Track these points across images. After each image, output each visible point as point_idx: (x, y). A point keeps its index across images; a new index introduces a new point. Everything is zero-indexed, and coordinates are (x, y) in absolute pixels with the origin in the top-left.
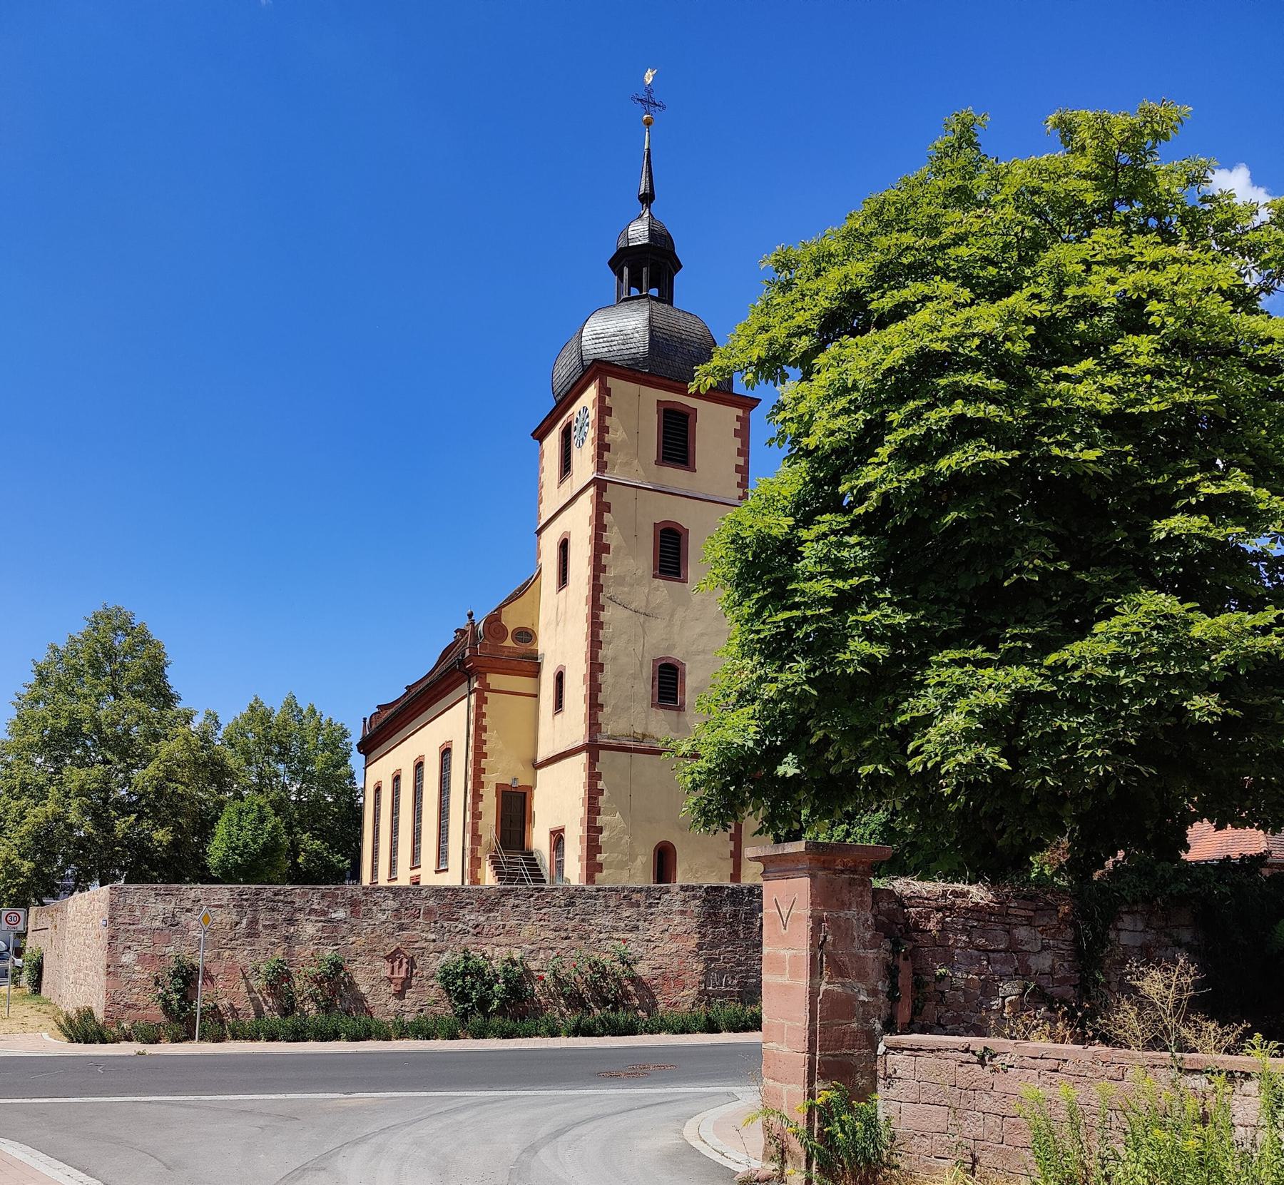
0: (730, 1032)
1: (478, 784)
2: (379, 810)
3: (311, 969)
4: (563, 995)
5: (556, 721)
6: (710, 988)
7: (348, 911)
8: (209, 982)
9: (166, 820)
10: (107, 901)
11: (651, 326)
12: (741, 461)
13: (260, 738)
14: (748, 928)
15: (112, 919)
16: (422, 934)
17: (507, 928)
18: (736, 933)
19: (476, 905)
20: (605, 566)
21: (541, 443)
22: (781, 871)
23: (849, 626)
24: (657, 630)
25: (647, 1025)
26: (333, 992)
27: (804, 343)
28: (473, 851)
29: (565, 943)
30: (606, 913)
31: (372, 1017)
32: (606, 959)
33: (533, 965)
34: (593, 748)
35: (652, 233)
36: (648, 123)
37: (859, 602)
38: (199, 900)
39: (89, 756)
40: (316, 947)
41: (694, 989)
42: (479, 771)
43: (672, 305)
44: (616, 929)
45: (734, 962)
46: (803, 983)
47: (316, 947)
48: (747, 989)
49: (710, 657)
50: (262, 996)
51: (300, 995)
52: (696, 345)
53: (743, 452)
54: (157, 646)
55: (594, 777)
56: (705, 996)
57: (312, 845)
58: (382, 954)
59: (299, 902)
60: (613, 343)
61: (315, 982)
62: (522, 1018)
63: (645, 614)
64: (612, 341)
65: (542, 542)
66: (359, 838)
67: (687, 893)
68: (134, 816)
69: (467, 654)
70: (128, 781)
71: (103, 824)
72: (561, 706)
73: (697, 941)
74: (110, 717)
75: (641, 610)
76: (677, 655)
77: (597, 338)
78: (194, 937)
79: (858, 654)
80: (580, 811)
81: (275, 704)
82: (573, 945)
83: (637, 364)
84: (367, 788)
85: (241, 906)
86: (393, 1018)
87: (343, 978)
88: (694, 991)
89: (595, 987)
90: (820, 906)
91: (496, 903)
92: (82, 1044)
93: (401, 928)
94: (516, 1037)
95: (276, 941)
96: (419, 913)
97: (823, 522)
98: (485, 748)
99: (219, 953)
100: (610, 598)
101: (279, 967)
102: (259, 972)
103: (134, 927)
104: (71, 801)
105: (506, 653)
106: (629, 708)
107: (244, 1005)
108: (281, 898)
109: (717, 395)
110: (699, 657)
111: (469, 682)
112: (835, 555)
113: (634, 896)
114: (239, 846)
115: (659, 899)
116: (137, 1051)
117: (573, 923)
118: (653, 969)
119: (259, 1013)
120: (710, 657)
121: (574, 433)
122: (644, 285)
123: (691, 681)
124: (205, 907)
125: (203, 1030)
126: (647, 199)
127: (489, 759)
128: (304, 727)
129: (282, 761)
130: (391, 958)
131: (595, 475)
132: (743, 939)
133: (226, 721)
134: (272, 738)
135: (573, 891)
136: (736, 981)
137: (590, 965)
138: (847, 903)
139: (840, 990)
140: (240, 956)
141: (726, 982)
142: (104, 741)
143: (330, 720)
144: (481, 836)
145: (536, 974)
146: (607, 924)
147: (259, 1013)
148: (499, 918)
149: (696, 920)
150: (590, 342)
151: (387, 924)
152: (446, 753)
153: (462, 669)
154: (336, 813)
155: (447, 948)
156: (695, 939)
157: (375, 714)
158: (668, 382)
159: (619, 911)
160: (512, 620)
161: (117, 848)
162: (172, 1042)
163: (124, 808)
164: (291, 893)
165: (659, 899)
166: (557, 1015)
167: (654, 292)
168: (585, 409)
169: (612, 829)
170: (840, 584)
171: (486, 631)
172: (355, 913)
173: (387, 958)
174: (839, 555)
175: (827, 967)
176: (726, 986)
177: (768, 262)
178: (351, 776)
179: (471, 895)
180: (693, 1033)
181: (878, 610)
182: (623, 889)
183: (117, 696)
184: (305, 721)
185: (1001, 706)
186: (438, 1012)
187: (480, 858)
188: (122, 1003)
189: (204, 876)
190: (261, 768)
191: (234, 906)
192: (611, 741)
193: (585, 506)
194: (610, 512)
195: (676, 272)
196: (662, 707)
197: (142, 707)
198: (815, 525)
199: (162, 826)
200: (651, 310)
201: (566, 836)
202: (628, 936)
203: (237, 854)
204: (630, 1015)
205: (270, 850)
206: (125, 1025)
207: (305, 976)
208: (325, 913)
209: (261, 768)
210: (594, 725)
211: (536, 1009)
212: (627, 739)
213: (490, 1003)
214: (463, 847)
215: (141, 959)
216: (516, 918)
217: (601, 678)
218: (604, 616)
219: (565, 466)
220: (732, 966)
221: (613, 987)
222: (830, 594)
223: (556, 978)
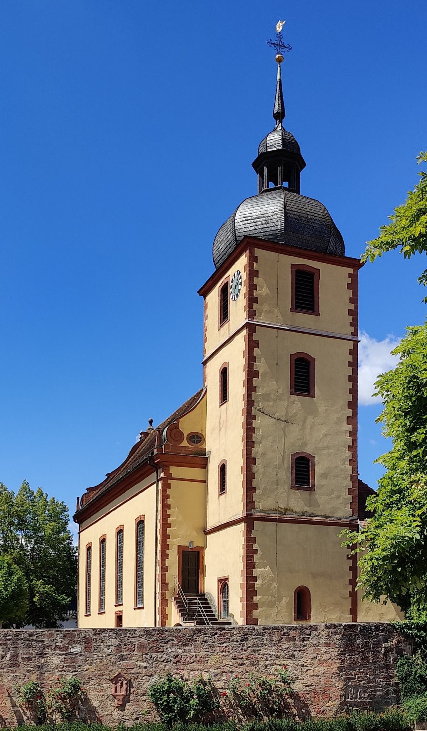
1: (165, 547)
2: (90, 563)
3: (58, 689)
4: (241, 706)
5: (221, 501)
6: (349, 700)
7: (83, 647)
11: (286, 209)
12: (352, 307)
13: (5, 513)
14: (376, 655)
16: (137, 663)
17: (198, 658)
18: (366, 658)
19: (175, 641)
20: (256, 387)
24: (294, 432)
26: (74, 706)
28: (162, 595)
29: (241, 669)
30: (270, 645)
31: (102, 724)
32: (272, 680)
33: (218, 685)
35: (284, 141)
36: (279, 61)
40: (60, 673)
41: (337, 700)
42: (165, 537)
44: (278, 657)
47: (60, 673)
48: (375, 700)
49: (332, 451)
50: (22, 709)
51: (50, 709)
52: (319, 222)
53: (354, 300)
55: (250, 541)
57: (44, 588)
58: (108, 677)
59: (47, 641)
60: (258, 224)
61: (60, 699)
62: (211, 724)
63: (285, 421)
64: (257, 222)
65: (207, 369)
66: (76, 582)
67: (330, 630)
69: (155, 452)
72: (224, 489)
73: (339, 665)
75: (282, 419)
76: (308, 450)
77: (246, 220)
80: (241, 566)
82: (247, 669)
83: (276, 238)
85: (6, 644)
86: (117, 724)
87: (80, 696)
88: (337, 702)
89: (263, 700)
91: (190, 639)
93: (122, 658)
95: (32, 669)
96: (134, 647)
98: (170, 521)
100: (259, 410)
101: (34, 688)
102: (20, 692)
105: (183, 451)
106: (275, 490)
108: (34, 638)
109: (335, 258)
110: (325, 451)
111: (157, 473)
113: (291, 632)
115: (310, 635)
117: (247, 653)
118: (306, 686)
119: (21, 722)
120: (332, 451)
121: (230, 290)
123: (319, 469)
126: (279, 116)
127: (172, 528)
128: (35, 504)
129: (21, 529)
130: (115, 680)
131: (247, 321)
132: (372, 663)
134: (13, 513)
135: (246, 630)
136: (367, 694)
137: (260, 684)
140: (6, 680)
141: (360, 695)
143: (54, 499)
144: (168, 584)
145: (220, 691)
146: (272, 653)
148: (193, 651)
149: (337, 650)
150: (241, 223)
151: (111, 656)
152: (140, 523)
153: (152, 464)
154: (61, 565)
155: (155, 672)
157: (85, 494)
158: (297, 250)
159: (280, 644)
165: (310, 635)
166: (236, 721)
167: (286, 184)
168: (239, 273)
169: (264, 578)
171: (169, 437)
172: (87, 649)
173: (111, 680)
176: (360, 698)
178: (69, 538)
179: (172, 634)
182: (283, 628)
184: (36, 500)
185: (419, 448)
186: (150, 720)
187: (168, 600)
190: (6, 535)
192: (262, 514)
194: (258, 348)
200: (285, 198)
201: (231, 583)
207: (53, 695)
208: (66, 649)
209: (6, 535)
210: (250, 503)
211: (221, 716)
212: (274, 512)
213: (187, 713)
214: (155, 592)
216: (205, 650)
217: (254, 469)
218: (255, 424)
219: (224, 315)
220: (364, 683)
221: (277, 700)
223: (235, 693)
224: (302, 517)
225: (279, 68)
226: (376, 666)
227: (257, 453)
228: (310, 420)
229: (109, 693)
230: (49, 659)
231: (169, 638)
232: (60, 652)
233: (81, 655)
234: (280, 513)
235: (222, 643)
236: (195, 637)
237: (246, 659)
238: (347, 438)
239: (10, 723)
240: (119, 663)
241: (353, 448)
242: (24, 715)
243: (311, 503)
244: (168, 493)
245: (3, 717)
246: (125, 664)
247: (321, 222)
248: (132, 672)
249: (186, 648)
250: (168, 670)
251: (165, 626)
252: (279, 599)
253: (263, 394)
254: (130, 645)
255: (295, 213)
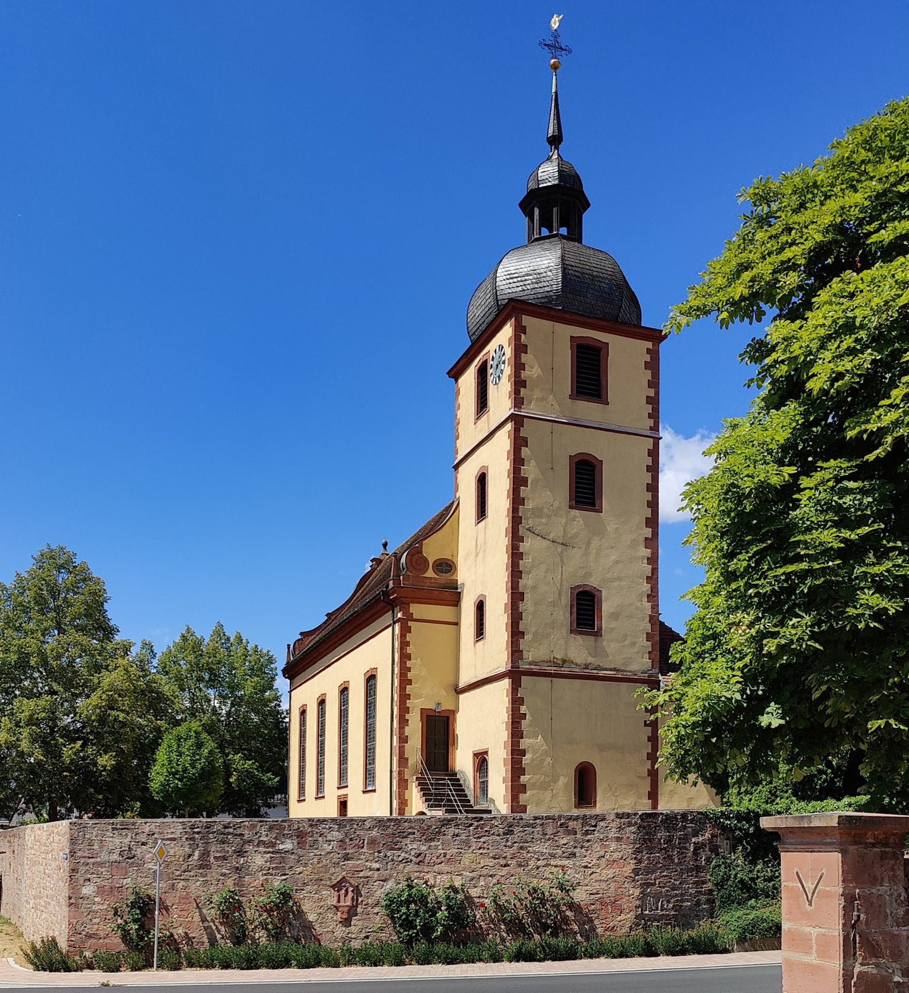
0: (668, 955)
1: (404, 710)
2: (305, 732)
3: (262, 898)
4: (504, 921)
7: (295, 842)
8: (164, 912)
9: (108, 746)
10: (67, 836)
11: (563, 264)
12: (651, 392)
14: (683, 853)
15: (72, 853)
16: (367, 864)
17: (448, 857)
18: (670, 858)
19: (417, 835)
21: (457, 380)
22: (803, 844)
23: (856, 578)
24: (575, 557)
25: (586, 950)
26: (283, 920)
27: (792, 279)
28: (400, 773)
29: (505, 871)
30: (543, 840)
31: (320, 944)
32: (545, 886)
33: (474, 892)
34: (515, 675)
36: (555, 67)
37: (865, 553)
38: (153, 834)
39: (37, 687)
40: (265, 877)
41: (631, 913)
42: (404, 697)
43: (580, 242)
44: (553, 856)
45: (669, 887)
46: (836, 964)
47: (265, 877)
48: (682, 913)
49: (625, 583)
50: (215, 925)
52: (607, 281)
53: (654, 383)
54: (98, 582)
55: (516, 702)
56: (643, 922)
57: (243, 765)
58: (328, 883)
59: (247, 835)
61: (265, 911)
62: (465, 944)
63: (562, 544)
64: (526, 280)
65: (459, 476)
66: (286, 757)
67: (622, 820)
68: (80, 743)
69: (391, 585)
70: (73, 710)
71: (52, 751)
72: (482, 634)
73: (633, 867)
74: (55, 651)
75: (558, 541)
76: (593, 582)
77: (511, 278)
78: (149, 869)
79: (871, 608)
81: (204, 632)
82: (512, 872)
83: (550, 302)
84: (292, 711)
85: (193, 839)
86: (340, 944)
87: (292, 907)
88: (631, 915)
89: (534, 912)
90: (852, 883)
92: (47, 973)
93: (346, 858)
94: (459, 963)
96: (363, 843)
97: (827, 468)
99: (173, 884)
100: (529, 530)
101: (230, 897)
103: (93, 860)
104: (22, 730)
107: (198, 933)
108: (231, 830)
110: (615, 584)
111: (393, 612)
112: (836, 502)
114: (179, 771)
115: (595, 826)
116: (102, 982)
117: (512, 851)
118: (591, 894)
119: (213, 941)
120: (625, 583)
121: (490, 371)
122: (555, 224)
123: (607, 607)
124: (159, 841)
125: (160, 958)
126: (555, 141)
128: (232, 653)
130: (337, 887)
131: (512, 411)
132: (677, 864)
133: (160, 649)
134: (203, 665)
135: (511, 820)
136: (671, 905)
138: (879, 877)
139: (875, 971)
141: (662, 906)
142: (50, 673)
143: (256, 646)
144: (407, 759)
145: (476, 900)
146: (545, 851)
147: (213, 941)
149: (631, 847)
150: (504, 282)
151: (332, 854)
152: (371, 679)
153: (386, 600)
154: (266, 735)
155: (391, 876)
156: (632, 865)
157: (298, 640)
158: (580, 318)
159: (556, 838)
160: (432, 550)
161: (65, 774)
162: (132, 970)
163: (70, 736)
164: (237, 826)
165: (595, 826)
166: (498, 941)
167: (564, 231)
168: (501, 347)
169: (535, 752)
170: (846, 534)
171: (409, 564)
172: (301, 844)
173: (333, 887)
174: (841, 501)
175: (860, 948)
176: (662, 910)
177: (744, 199)
178: (277, 698)
179: (413, 825)
180: (631, 957)
181: (888, 560)
182: (560, 817)
183: (61, 631)
184: (233, 648)
188: (84, 933)
189: (152, 810)
190: (193, 694)
191: (187, 839)
192: (532, 667)
193: (503, 441)
194: (527, 447)
195: (585, 210)
196: (581, 633)
197: (84, 639)
198: (817, 471)
199: (106, 752)
200: (563, 249)
201: (490, 759)
202: (565, 862)
203: (177, 779)
204: (571, 942)
205: (208, 774)
206: (87, 953)
207: (256, 906)
208: (273, 845)
209: (193, 694)
210: (516, 652)
211: (478, 934)
212: (548, 664)
213: (433, 929)
214: (391, 770)
215: (101, 890)
216: (456, 847)
217: (522, 606)
218: (523, 547)
219: (482, 403)
220: (667, 891)
221: (552, 912)
222: (836, 545)
223: (497, 904)
224: (586, 671)
225: (554, 77)
226: (684, 867)
227: (525, 586)
228: (595, 542)
229: (329, 904)
230: (250, 858)
231: (410, 830)
232: (265, 850)
233: (293, 853)
234: (555, 664)
235: (480, 838)
236: (443, 829)
237: (511, 858)
238: (644, 567)
239: (198, 943)
240: (343, 863)
241: (653, 579)
242: (216, 932)
243: (597, 652)
244: (408, 639)
245: (190, 935)
246: (351, 865)
247: (611, 280)
248: (360, 875)
249: (432, 844)
250: (408, 873)
251: (403, 814)
252: (555, 779)
253: (533, 508)
254: (358, 840)
255: (576, 269)
